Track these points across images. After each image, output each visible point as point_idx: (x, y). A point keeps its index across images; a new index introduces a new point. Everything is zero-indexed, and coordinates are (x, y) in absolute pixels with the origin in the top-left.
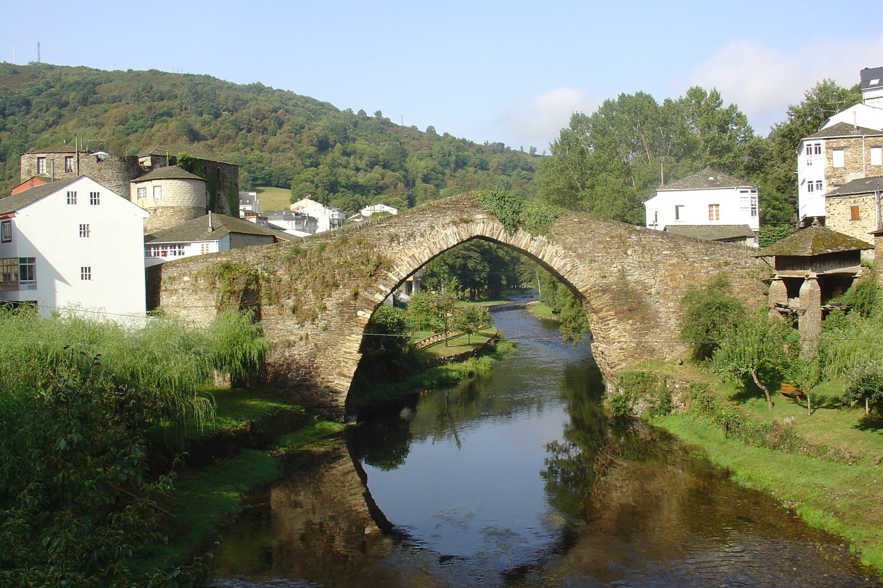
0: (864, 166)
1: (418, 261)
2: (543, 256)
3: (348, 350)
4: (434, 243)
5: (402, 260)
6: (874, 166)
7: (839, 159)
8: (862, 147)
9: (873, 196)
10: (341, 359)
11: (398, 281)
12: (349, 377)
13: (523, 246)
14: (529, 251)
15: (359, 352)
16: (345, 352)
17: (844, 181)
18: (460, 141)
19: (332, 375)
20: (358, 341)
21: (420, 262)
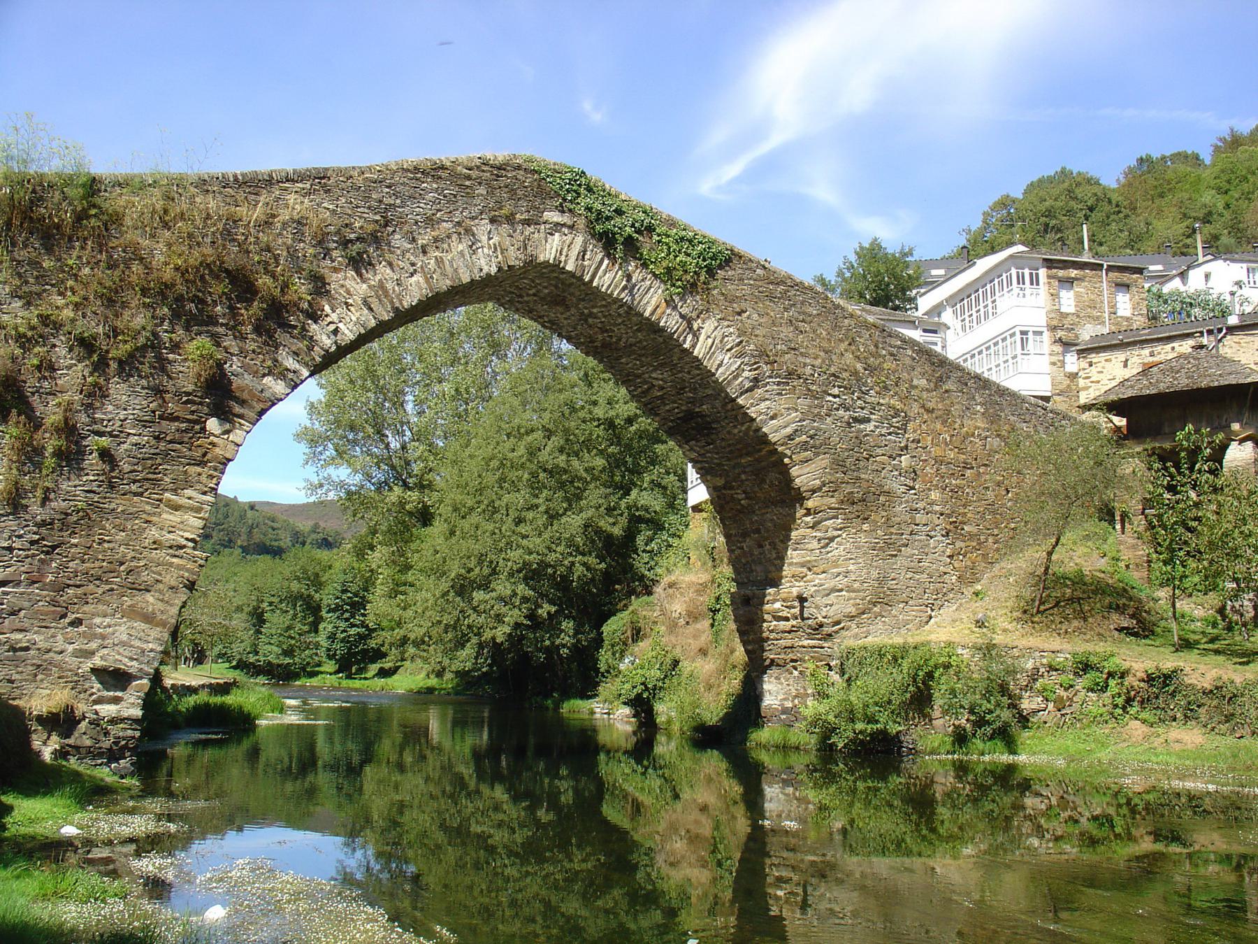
0: (1106, 315)
5: (348, 292)
6: (1121, 317)
7: (1068, 302)
8: (1102, 282)
11: (333, 348)
17: (1077, 337)
20: (199, 510)
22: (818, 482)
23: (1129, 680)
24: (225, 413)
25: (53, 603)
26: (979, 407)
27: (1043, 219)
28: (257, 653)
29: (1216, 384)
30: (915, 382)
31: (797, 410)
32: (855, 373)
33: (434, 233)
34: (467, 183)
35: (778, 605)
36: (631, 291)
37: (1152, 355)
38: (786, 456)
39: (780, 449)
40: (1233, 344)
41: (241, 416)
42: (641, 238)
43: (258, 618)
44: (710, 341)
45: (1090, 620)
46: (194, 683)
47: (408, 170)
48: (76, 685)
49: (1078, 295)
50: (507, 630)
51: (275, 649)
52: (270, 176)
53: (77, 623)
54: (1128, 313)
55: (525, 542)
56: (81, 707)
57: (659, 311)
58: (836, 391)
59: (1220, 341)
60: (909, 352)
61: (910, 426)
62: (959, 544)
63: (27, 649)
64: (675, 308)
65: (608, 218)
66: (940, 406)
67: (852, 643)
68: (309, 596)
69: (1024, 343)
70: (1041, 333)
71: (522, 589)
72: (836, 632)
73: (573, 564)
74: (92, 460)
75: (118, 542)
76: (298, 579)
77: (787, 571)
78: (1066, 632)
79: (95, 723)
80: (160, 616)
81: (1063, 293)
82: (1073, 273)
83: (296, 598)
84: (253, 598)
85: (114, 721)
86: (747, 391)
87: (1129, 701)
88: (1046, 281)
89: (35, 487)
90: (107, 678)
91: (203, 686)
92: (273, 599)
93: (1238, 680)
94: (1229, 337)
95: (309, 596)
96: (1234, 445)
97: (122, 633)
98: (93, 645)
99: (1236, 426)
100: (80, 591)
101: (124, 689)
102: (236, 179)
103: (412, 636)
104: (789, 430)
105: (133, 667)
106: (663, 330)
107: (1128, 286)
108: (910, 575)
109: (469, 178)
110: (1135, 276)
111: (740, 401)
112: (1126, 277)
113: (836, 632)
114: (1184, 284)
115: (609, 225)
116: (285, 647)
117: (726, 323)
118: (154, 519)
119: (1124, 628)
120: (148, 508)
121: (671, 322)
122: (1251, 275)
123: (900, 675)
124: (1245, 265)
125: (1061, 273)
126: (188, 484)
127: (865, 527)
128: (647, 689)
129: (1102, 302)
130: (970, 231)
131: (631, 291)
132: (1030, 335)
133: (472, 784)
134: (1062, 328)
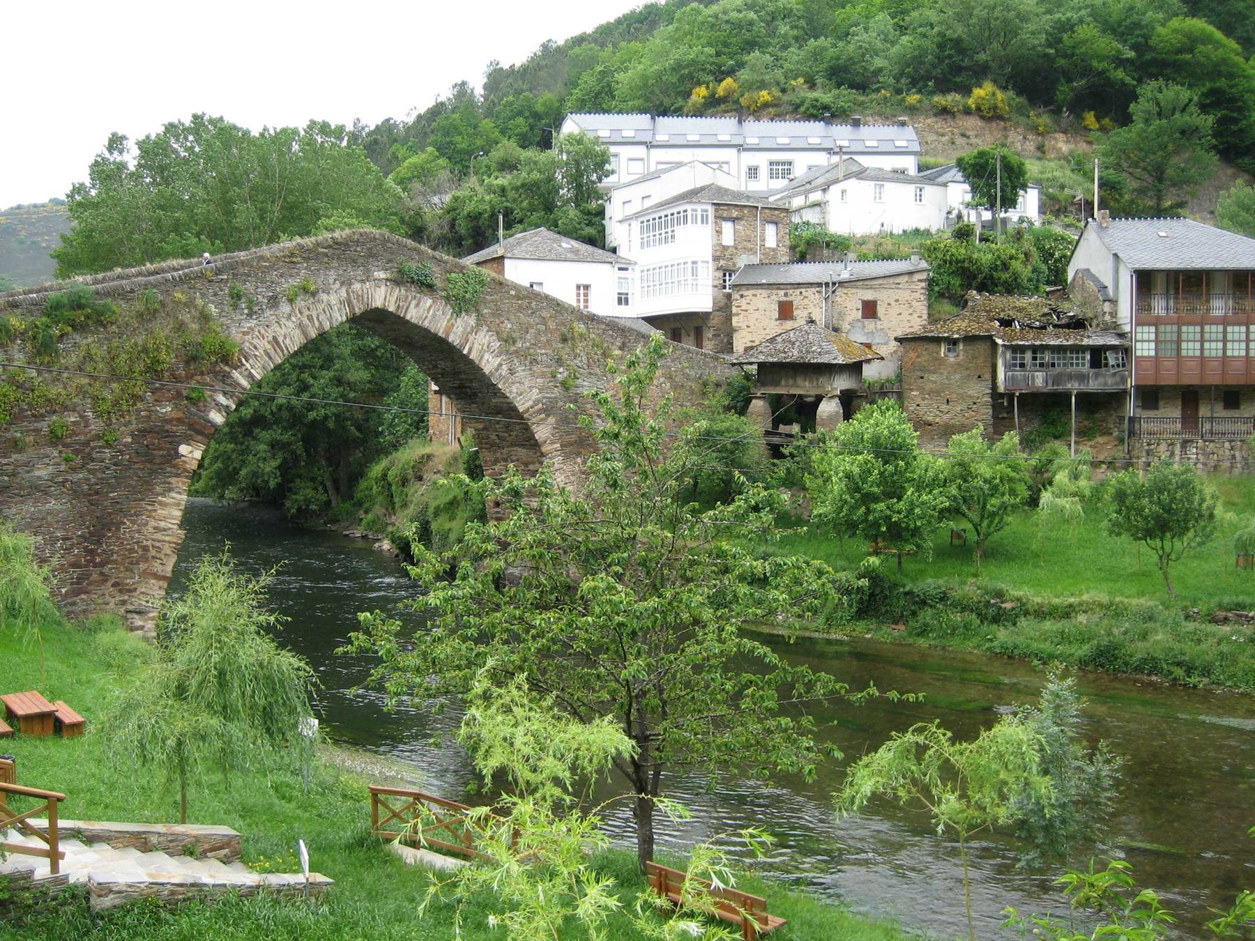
1: (282, 351)
2: (470, 350)
3: (162, 524)
4: (310, 318)
5: (255, 348)
10: (149, 543)
13: (441, 330)
14: (450, 340)
15: (181, 526)
16: (155, 528)
17: (734, 265)
18: (29, 206)
19: (131, 578)
20: (178, 505)
21: (285, 351)
54: (773, 245)
70: (707, 262)
126: (170, 490)
129: (756, 236)
132: (699, 265)
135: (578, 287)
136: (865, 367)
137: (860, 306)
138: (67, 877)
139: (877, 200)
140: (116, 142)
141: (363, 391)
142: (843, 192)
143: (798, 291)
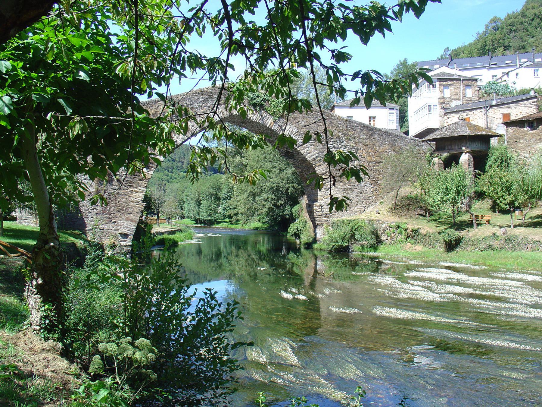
0: (461, 97)
7: (447, 93)
9: (481, 110)
12: (135, 222)
17: (450, 106)
20: (142, 192)
22: (324, 171)
23: (408, 231)
24: (147, 166)
25: (109, 218)
26: (387, 142)
27: (510, 27)
28: (199, 215)
29: (456, 135)
30: (361, 137)
31: (317, 150)
32: (339, 136)
33: (202, 111)
34: (211, 94)
35: (317, 208)
36: (262, 120)
37: (467, 115)
38: (313, 164)
39: (311, 162)
40: (492, 112)
41: (152, 167)
42: (265, 104)
43: (199, 203)
44: (288, 132)
45: (410, 212)
46: (163, 231)
47: (194, 93)
48: (115, 237)
49: (451, 91)
50: (266, 210)
51: (205, 214)
52: (156, 100)
53: (114, 222)
55: (272, 180)
56: (117, 243)
57: (271, 125)
58: (331, 143)
59: (487, 111)
60: (359, 127)
61: (359, 151)
62: (375, 187)
63: (103, 229)
64: (277, 123)
65: (254, 99)
66: (371, 144)
67: (335, 219)
68: (216, 194)
69: (430, 110)
71: (271, 196)
72: (331, 216)
73: (289, 186)
74: (115, 181)
75: (122, 202)
76: (212, 188)
77: (319, 197)
78: (401, 216)
79: (120, 246)
80: (134, 220)
81: (446, 90)
82: (449, 83)
83: (212, 195)
84: (197, 195)
85: (125, 246)
86: (300, 146)
87: (408, 237)
88: (439, 86)
89: (102, 190)
90: (123, 236)
91: (166, 232)
92: (203, 196)
93: (431, 232)
94: (491, 109)
95: (216, 194)
96: (463, 154)
97: (125, 224)
98: (119, 228)
99: (464, 148)
100: (114, 215)
101: (127, 238)
102: (146, 103)
103: (240, 211)
104: (314, 156)
105: (129, 233)
106: (273, 130)
107: (471, 86)
108: (357, 198)
109: (212, 93)
110: (473, 82)
111: (298, 149)
112: (470, 83)
113: (331, 216)
114: (508, 77)
115: (254, 101)
116: (208, 213)
117: (293, 126)
118: (131, 195)
119: (420, 214)
120: (130, 193)
121: (275, 127)
122: (536, 72)
123: (348, 229)
124: (533, 69)
125: (444, 83)
127: (341, 184)
128: (298, 230)
129: (460, 93)
130: (479, 33)
131: (262, 120)
132: (432, 107)
133: (257, 262)
134: (444, 103)
135: (370, 118)
136: (336, 109)
137: (502, 117)
138: (236, 54)
139: (536, 76)
140: (394, 66)
141: (379, 402)
142: (517, 74)
143: (472, 112)
